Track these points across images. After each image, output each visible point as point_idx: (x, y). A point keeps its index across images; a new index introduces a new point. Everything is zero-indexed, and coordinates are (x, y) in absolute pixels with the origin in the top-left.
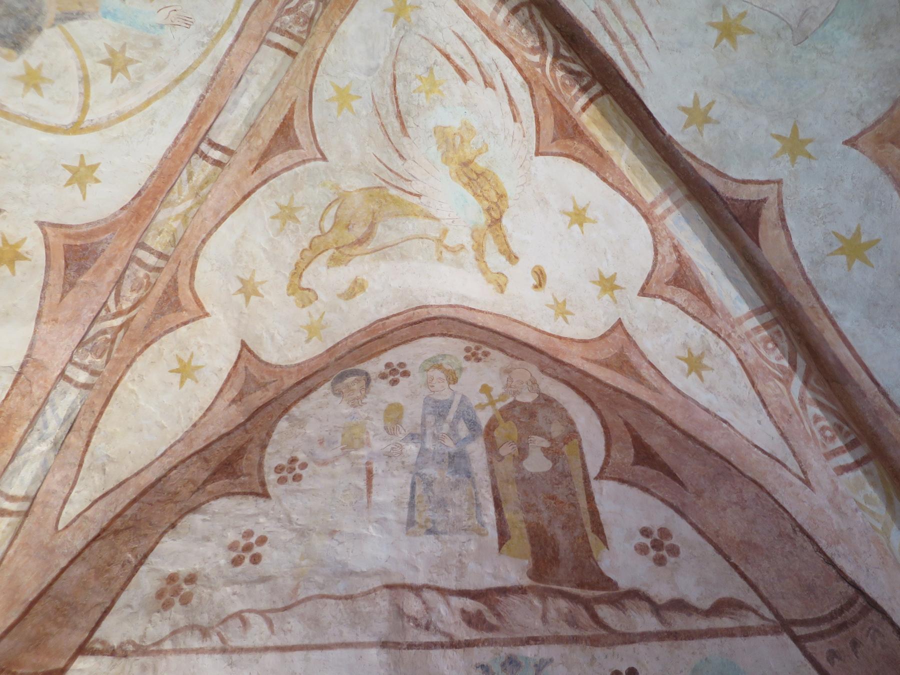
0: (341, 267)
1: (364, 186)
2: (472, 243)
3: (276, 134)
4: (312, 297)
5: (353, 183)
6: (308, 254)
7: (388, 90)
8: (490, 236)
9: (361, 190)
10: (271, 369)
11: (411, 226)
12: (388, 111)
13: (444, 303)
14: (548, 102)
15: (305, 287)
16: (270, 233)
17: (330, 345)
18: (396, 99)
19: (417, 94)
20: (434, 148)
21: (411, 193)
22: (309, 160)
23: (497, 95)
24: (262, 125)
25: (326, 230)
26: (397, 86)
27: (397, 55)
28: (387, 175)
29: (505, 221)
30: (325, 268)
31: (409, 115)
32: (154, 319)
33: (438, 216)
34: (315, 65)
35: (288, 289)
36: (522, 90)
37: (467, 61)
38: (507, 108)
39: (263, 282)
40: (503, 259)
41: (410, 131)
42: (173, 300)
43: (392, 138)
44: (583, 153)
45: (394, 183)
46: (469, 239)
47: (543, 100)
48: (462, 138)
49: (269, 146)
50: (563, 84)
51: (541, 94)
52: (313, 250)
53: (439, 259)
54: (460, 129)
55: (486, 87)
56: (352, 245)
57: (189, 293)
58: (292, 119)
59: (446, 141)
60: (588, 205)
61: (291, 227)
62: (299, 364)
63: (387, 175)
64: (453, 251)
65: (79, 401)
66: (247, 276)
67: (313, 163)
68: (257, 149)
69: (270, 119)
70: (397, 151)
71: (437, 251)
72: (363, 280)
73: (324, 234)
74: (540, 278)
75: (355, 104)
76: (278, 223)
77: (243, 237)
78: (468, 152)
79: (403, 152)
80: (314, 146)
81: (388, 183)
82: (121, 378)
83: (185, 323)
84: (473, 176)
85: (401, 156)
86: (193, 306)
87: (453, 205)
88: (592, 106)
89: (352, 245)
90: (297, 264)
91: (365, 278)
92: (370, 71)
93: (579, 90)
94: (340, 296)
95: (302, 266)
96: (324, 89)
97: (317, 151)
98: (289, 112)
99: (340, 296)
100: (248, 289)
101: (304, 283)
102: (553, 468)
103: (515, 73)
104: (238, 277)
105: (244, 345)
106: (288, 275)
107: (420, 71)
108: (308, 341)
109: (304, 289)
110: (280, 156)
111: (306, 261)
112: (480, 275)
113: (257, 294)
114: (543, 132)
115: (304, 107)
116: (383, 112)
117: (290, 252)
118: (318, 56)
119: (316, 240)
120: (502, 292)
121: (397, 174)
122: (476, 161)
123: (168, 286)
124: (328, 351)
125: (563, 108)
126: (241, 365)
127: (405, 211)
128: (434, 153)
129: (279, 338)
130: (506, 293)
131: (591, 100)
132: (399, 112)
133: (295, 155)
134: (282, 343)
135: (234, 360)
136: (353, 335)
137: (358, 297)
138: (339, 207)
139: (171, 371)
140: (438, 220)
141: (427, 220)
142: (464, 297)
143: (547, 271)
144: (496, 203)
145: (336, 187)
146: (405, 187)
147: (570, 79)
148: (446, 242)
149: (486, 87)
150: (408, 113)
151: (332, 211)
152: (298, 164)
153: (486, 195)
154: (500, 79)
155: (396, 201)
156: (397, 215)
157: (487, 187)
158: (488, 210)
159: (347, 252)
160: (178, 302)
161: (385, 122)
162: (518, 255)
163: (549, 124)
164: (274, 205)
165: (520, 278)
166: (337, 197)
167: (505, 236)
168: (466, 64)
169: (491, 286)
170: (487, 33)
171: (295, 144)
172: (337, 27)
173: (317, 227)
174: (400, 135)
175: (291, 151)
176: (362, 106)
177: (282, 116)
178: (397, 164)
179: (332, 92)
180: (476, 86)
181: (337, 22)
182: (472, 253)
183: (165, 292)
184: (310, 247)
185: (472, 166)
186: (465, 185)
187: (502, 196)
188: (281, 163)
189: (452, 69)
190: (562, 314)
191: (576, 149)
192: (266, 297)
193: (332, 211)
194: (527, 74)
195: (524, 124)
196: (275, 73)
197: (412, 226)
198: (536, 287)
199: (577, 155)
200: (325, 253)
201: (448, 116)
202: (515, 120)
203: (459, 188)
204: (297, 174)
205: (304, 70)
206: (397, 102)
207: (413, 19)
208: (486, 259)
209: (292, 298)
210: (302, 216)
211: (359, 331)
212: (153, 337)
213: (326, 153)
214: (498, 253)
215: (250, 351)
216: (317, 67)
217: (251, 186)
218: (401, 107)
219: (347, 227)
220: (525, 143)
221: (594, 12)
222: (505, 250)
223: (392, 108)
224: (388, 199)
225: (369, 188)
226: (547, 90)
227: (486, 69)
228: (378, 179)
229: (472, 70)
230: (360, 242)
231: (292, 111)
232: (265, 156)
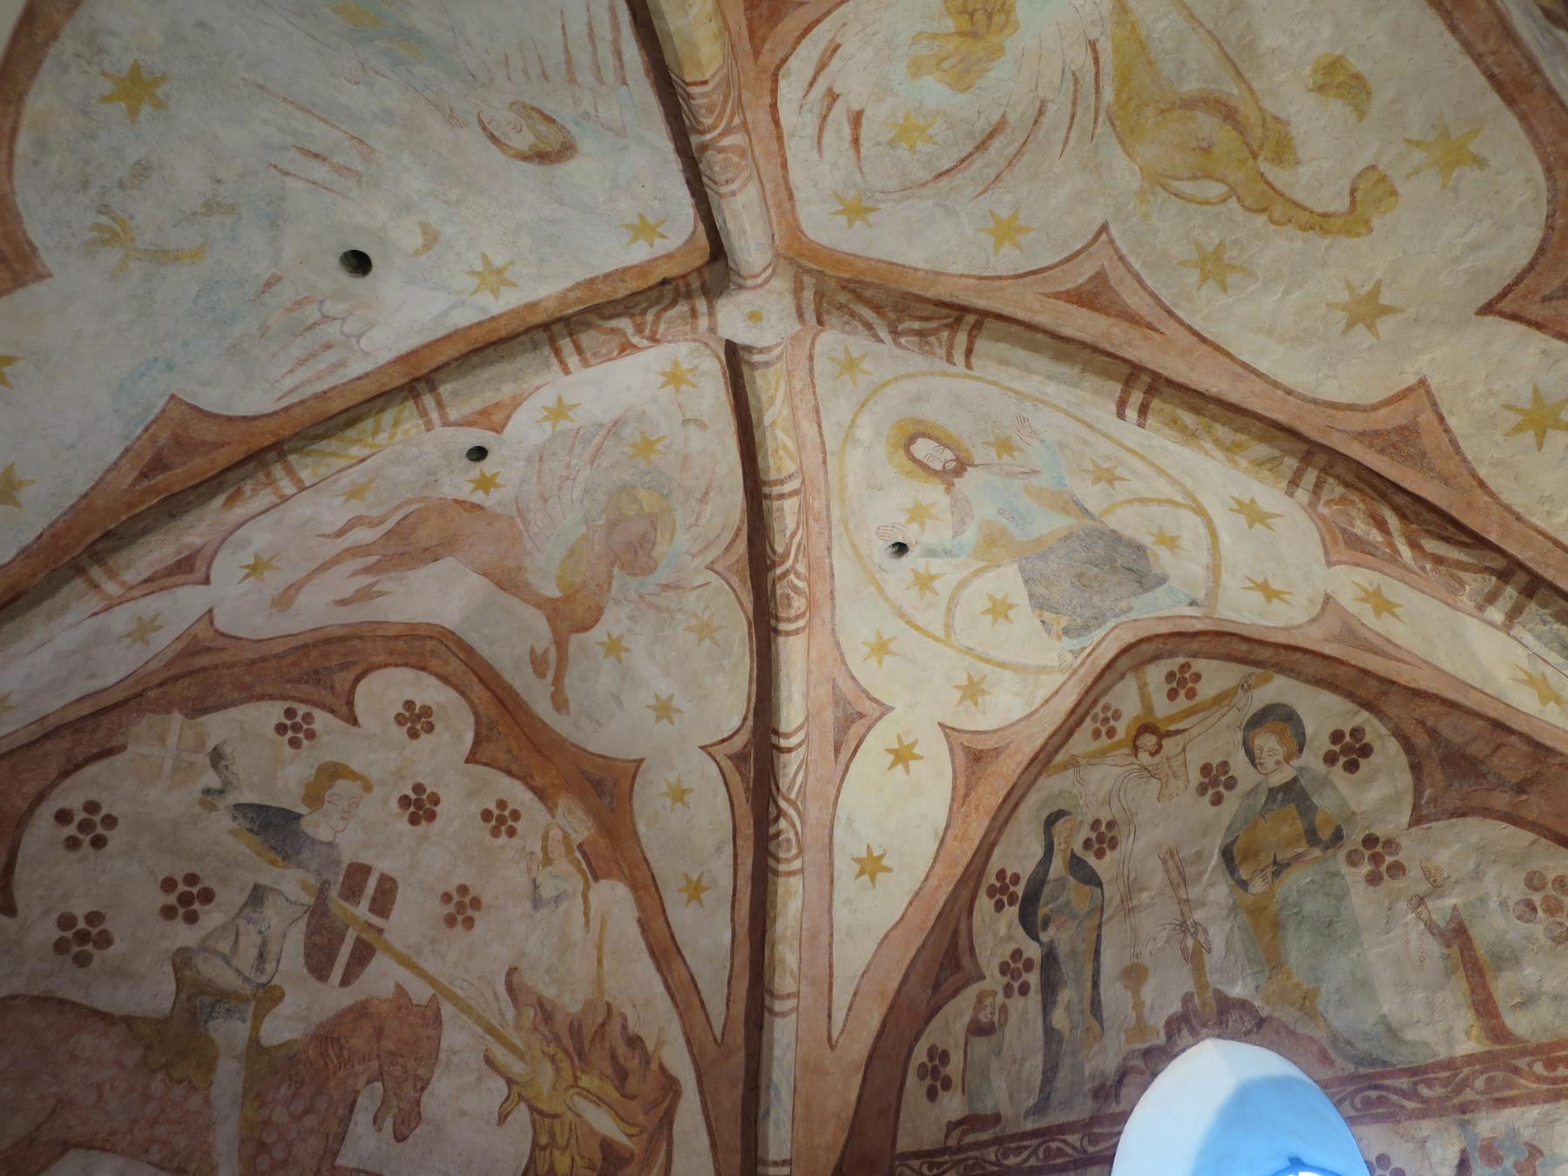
1: (1120, 151)
3: (1096, 310)
4: (1374, 177)
5: (1124, 172)
6: (1278, 212)
7: (959, 179)
9: (1128, 154)
10: (1556, 238)
11: (1161, 25)
12: (987, 165)
15: (1347, 200)
16: (1252, 288)
17: (1494, 99)
18: (962, 161)
20: (992, 74)
21: (1096, 60)
22: (1117, 250)
25: (1223, 189)
27: (908, 189)
28: (1085, 118)
30: (1302, 169)
32: (1432, 469)
35: (1358, 235)
39: (1349, 286)
41: (995, 118)
42: (1394, 438)
45: (1092, 99)
51: (769, 57)
52: (1270, 203)
56: (1240, 128)
57: (1383, 412)
58: (1067, 292)
61: (1234, 253)
62: (1549, 170)
63: (1085, 118)
65: (1540, 627)
66: (1341, 316)
67: (1119, 243)
70: (1036, 122)
72: (1315, 71)
73: (1233, 191)
75: (1004, 213)
76: (1233, 279)
77: (1270, 332)
81: (1097, 111)
82: (1540, 532)
83: (1441, 419)
85: (1041, 112)
86: (1407, 406)
89: (1240, 128)
90: (1303, 228)
91: (1308, 70)
94: (1362, 114)
95: (1304, 217)
99: (1362, 114)
100: (1367, 310)
101: (1340, 205)
104: (1345, 332)
105: (1488, 309)
106: (1327, 242)
107: (903, 152)
108: (1481, 162)
109: (1353, 202)
110: (1125, 297)
113: (1375, 293)
115: (1045, 279)
116: (992, 172)
117: (1284, 245)
118: (973, 281)
121: (1074, 103)
123: (1371, 445)
124: (1510, 101)
126: (1536, 311)
127: (1136, 50)
128: (1000, 71)
129: (1473, 233)
132: (977, 148)
133: (1116, 275)
134: (1487, 223)
135: (1520, 328)
136: (1467, 46)
137: (1357, 64)
138: (1175, 178)
139: (1540, 446)
146: (1090, 77)
150: (971, 134)
151: (1187, 187)
152: (1129, 268)
156: (1150, 63)
159: (1258, 132)
160: (1401, 430)
164: (1204, 292)
166: (1158, 189)
170: (780, 138)
171: (1100, 277)
172: (927, 272)
174: (1008, 130)
175: (1112, 283)
177: (1070, 306)
178: (1058, 111)
181: (921, 273)
183: (1382, 451)
184: (1264, 210)
185: (969, 28)
192: (1379, 275)
193: (1187, 187)
200: (1270, 177)
202: (838, 46)
204: (1144, 264)
207: (853, 193)
209: (1376, 222)
210: (1212, 238)
211: (1454, 29)
212: (1465, 473)
213: (1095, 228)
215: (1503, 295)
216: (987, 278)
217: (1184, 332)
221: (624, 83)
223: (979, 161)
224: (1125, 97)
225: (1122, 142)
228: (1098, 131)
230: (1229, 114)
231: (1057, 296)
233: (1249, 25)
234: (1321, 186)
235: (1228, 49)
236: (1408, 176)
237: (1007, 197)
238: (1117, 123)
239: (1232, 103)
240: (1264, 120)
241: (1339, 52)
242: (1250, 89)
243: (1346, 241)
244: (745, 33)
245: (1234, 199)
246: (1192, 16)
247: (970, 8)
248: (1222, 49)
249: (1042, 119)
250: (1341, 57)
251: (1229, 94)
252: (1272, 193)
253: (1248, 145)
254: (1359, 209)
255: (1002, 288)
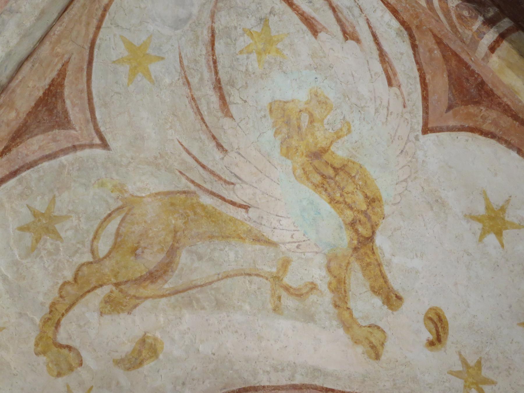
0: (122, 315)
1: (162, 189)
2: (329, 279)
3: (37, 105)
5: (146, 183)
7: (203, 50)
8: (356, 265)
11: (232, 255)
12: (201, 79)
13: (284, 382)
14: (437, 53)
15: (64, 342)
16: (16, 252)
18: (215, 62)
19: (245, 56)
20: (270, 133)
21: (233, 203)
22: (82, 147)
23: (362, 50)
24: (18, 91)
26: (216, 44)
28: (198, 174)
29: (379, 240)
30: (96, 315)
31: (233, 86)
33: (275, 239)
34: (100, 13)
35: (37, 345)
36: (398, 40)
37: (318, 6)
38: (377, 67)
40: (377, 301)
41: (233, 109)
43: (206, 119)
44: (495, 123)
45: (208, 186)
46: (324, 273)
47: (431, 51)
48: (311, 115)
49: (26, 121)
50: (460, 17)
51: (427, 43)
52: (79, 286)
53: (276, 309)
54: (307, 103)
55: (347, 39)
56: (140, 281)
59: (288, 123)
60: (508, 201)
61: (48, 245)
63: (198, 174)
64: (298, 294)
67: (87, 152)
68: (8, 125)
69: (31, 84)
70: (214, 138)
71: (272, 296)
72: (155, 339)
73: (98, 261)
74: (438, 327)
75: (155, 68)
76: (28, 238)
78: (321, 137)
79: (223, 140)
80: (91, 125)
81: (199, 186)
84: (328, 173)
85: (219, 146)
87: (299, 220)
88: (505, 44)
89: (140, 281)
90: (53, 305)
91: (158, 335)
92: (178, 23)
93: (484, 23)
94: (118, 363)
95: (62, 308)
96: (111, 45)
97: (94, 134)
98: (58, 75)
99: (118, 363)
101: (62, 337)
102: (484, 226)
103: (388, 16)
106: (38, 320)
107: (250, 23)
109: (61, 346)
110: (40, 137)
111: (68, 301)
112: (341, 331)
114: (433, 98)
116: (194, 81)
117: (44, 283)
119: (85, 269)
120: (377, 357)
121: (212, 173)
122: (332, 149)
125: (460, 61)
127: (223, 231)
128: (269, 139)
130: (383, 358)
131: (502, 36)
132: (218, 81)
133: (61, 137)
137: (147, 367)
138: (123, 220)
140: (274, 244)
141: (258, 247)
142: (316, 370)
143: (448, 315)
144: (365, 213)
145: (120, 188)
146: (225, 193)
147: (469, 9)
148: (287, 280)
149: (347, 39)
151: (113, 226)
152: (65, 151)
153: (348, 200)
154: (367, 27)
155: (211, 215)
156: (211, 237)
157: (350, 188)
158: (352, 224)
159: (132, 292)
161: (197, 94)
162: (401, 294)
163: (440, 85)
164: (25, 210)
165: (406, 330)
166: (120, 203)
167: (379, 265)
168: (316, 10)
169: (360, 349)
171: (64, 123)
173: (87, 249)
174: (220, 114)
175: (57, 131)
176: (164, 72)
177: (48, 81)
178: (213, 158)
179: (122, 51)
180: (331, 40)
182: (328, 297)
184: (75, 279)
185: (326, 157)
186: (316, 187)
187: (373, 200)
188: (40, 148)
189: (296, 19)
190: (476, 384)
191: (484, 118)
193: (113, 226)
194: (405, 17)
195: (403, 88)
196: (43, 13)
197: (234, 255)
198: (431, 344)
199: (486, 127)
200: (98, 291)
201: (291, 87)
202: (390, 84)
203: (307, 193)
205: (84, 18)
206: (215, 67)
208: (351, 304)
209: (43, 359)
210: (66, 230)
213: (108, 137)
214: (370, 293)
216: (103, 16)
218: (221, 74)
219: (134, 252)
220: (407, 116)
222: (381, 288)
224: (199, 210)
226: (435, 36)
227: (345, 14)
228: (184, 180)
229: (325, 18)
230: (152, 277)
231: (62, 74)
232: (19, 135)
233: (203, 308)
234: (80, 326)
235: (194, 291)
236: (68, 386)
237: (167, 81)
238: (183, 196)
239: (160, 281)
240: (138, 298)
241: (161, 356)
242: (163, 296)
243: (34, 335)
244: (463, 56)
245: (91, 260)
246: (227, 277)
247: (341, 173)
248: (196, 287)
249: (214, 143)
250: (157, 357)
251: (166, 282)
252: (86, 290)
253: (126, 282)
254: (55, 349)
255: (88, 24)
